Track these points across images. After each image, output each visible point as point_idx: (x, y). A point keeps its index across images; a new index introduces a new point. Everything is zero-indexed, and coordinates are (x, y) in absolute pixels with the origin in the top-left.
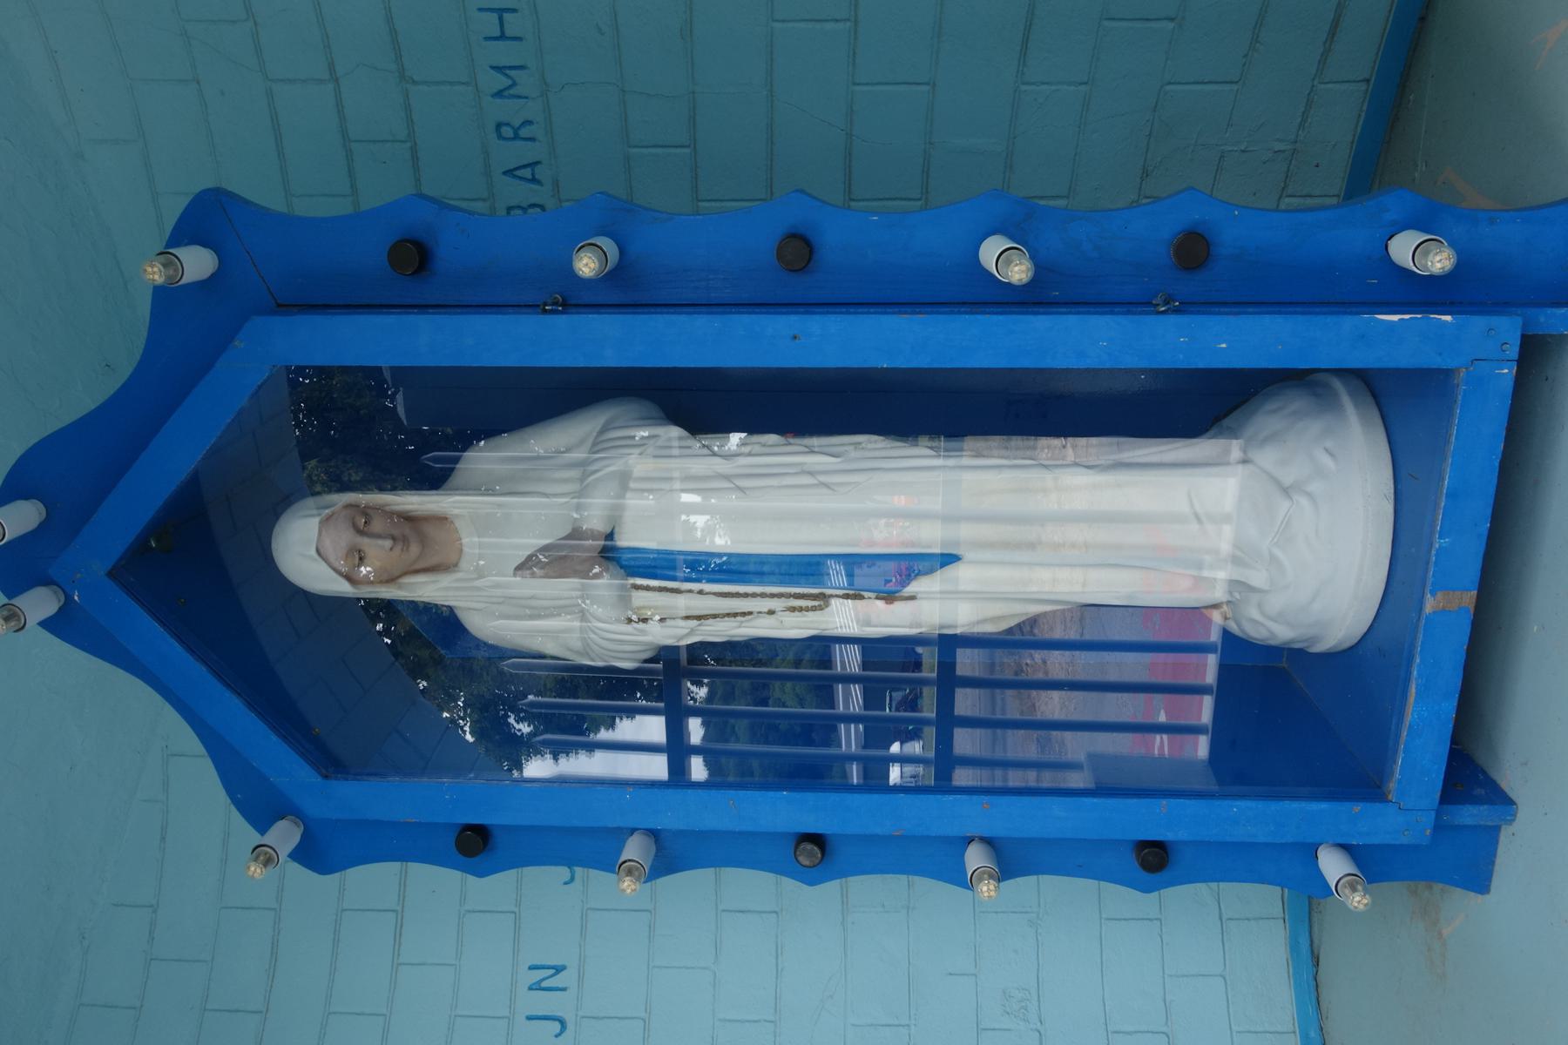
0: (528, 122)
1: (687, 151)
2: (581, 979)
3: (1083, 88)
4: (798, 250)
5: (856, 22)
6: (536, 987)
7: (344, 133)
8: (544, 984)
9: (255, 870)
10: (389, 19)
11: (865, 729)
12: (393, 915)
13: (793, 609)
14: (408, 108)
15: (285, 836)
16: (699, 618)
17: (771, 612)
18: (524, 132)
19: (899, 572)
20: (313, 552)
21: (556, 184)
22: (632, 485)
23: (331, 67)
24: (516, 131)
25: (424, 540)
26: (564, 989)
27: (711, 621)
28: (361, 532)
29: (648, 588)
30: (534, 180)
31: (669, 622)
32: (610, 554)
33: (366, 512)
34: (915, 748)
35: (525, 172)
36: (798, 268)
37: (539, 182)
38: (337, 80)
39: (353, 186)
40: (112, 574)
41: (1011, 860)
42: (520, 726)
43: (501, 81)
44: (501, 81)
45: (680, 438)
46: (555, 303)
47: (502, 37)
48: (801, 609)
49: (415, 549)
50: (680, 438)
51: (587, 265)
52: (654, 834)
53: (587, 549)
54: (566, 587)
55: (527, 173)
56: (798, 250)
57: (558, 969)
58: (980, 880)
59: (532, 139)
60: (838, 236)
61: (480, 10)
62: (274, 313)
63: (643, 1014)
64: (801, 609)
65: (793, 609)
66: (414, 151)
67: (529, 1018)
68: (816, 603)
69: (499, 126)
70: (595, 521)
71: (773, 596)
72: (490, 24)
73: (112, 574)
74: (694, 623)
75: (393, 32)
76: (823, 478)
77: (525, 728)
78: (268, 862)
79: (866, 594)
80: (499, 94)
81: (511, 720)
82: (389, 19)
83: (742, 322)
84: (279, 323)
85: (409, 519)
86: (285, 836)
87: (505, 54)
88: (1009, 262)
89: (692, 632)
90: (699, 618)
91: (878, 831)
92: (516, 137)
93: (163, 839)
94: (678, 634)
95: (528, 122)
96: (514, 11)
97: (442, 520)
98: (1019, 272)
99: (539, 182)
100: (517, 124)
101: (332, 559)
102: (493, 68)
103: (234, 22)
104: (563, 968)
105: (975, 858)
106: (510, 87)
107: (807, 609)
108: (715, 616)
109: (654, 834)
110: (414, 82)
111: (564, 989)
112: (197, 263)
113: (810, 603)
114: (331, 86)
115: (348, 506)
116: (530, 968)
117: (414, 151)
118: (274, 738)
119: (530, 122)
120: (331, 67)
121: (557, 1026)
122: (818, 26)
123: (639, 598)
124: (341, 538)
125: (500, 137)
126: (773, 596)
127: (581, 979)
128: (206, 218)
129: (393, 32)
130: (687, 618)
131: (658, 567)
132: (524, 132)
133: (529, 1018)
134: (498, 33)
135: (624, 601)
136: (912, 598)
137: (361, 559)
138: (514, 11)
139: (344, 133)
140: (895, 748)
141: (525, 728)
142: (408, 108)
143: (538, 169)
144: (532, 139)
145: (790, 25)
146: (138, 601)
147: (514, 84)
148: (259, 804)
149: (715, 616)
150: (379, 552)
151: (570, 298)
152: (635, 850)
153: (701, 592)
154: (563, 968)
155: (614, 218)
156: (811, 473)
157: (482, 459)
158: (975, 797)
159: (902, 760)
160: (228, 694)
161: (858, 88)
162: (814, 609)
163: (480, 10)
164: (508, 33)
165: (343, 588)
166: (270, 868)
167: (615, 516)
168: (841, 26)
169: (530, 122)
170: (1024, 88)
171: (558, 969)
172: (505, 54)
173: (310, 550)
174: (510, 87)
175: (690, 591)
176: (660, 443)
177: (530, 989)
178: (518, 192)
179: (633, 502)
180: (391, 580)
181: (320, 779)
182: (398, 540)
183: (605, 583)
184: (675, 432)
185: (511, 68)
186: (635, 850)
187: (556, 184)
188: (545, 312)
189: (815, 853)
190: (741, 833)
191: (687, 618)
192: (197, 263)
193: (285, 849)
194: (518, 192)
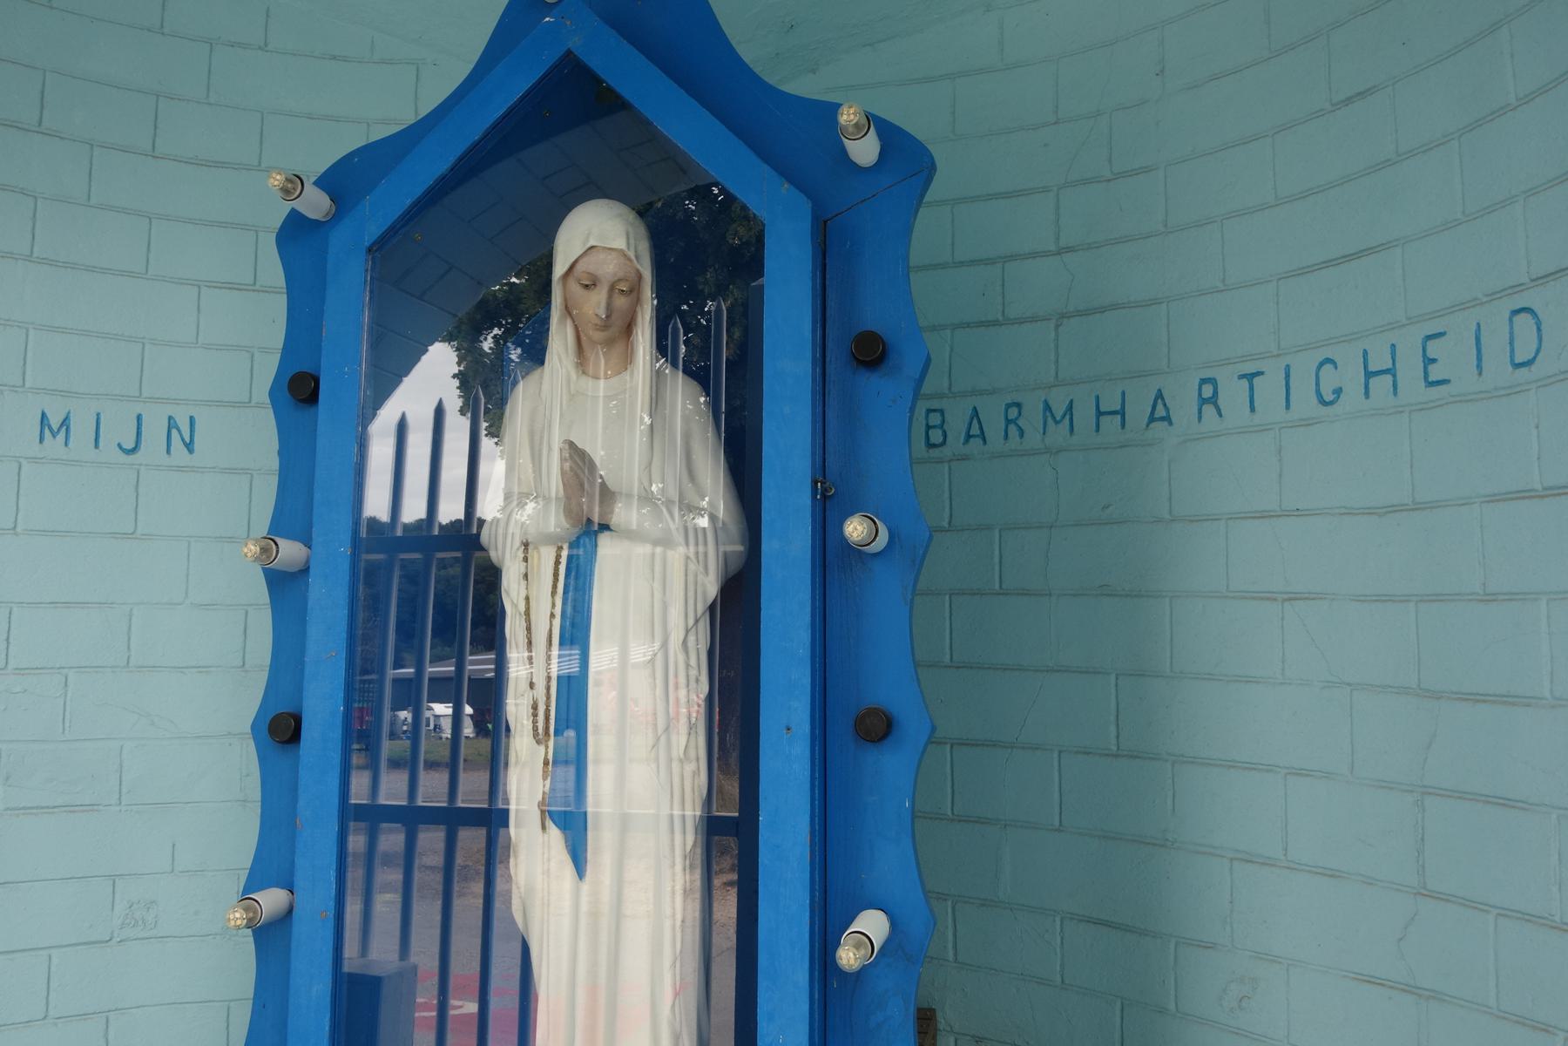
0: (1022, 433)
1: (997, 586)
2: (180, 469)
3: (1059, 979)
4: (877, 727)
5: (1116, 756)
6: (172, 424)
7: (1013, 257)
8: (174, 432)
9: (277, 180)
10: (1115, 307)
11: (489, 679)
12: (250, 280)
13: (535, 707)
14: (1034, 319)
15: (316, 204)
16: (527, 613)
17: (532, 685)
18: (1012, 429)
19: (571, 821)
20: (592, 243)
21: (965, 458)
22: (659, 550)
23: (1070, 249)
24: (1014, 421)
25: (609, 343)
26: (168, 451)
27: (524, 624)
28: (612, 288)
29: (557, 563)
30: (969, 437)
31: (523, 583)
32: (588, 531)
33: (634, 291)
34: (468, 730)
35: (976, 430)
36: (855, 727)
37: (967, 441)
38: (1059, 253)
39: (962, 264)
40: (569, 53)
41: (271, 936)
42: (490, 339)
43: (1059, 411)
44: (1059, 411)
45: (704, 593)
46: (825, 490)
47: (1099, 414)
48: (535, 715)
49: (598, 336)
50: (704, 593)
51: (855, 529)
52: (305, 571)
53: (591, 509)
54: (554, 485)
55: (975, 430)
56: (877, 727)
57: (189, 446)
58: (246, 910)
59: (1006, 436)
60: (890, 768)
61: (1123, 394)
62: (815, 218)
63: (139, 531)
64: (535, 715)
65: (535, 707)
66: (995, 323)
67: (139, 418)
68: (540, 731)
69: (1018, 405)
70: (625, 514)
71: (548, 688)
72: (1111, 402)
73: (569, 53)
74: (522, 608)
75: (1102, 310)
76: (663, 739)
77: (487, 345)
78: (286, 191)
79: (548, 782)
80: (1047, 407)
81: (496, 331)
82: (1115, 307)
83: (802, 677)
84: (805, 225)
85: (629, 329)
86: (316, 204)
87: (1085, 414)
88: (858, 946)
89: (515, 606)
90: (527, 613)
91: (301, 803)
92: (1008, 422)
93: (334, 58)
94: (512, 591)
95: (1022, 433)
96: (1123, 426)
97: (627, 360)
98: (848, 957)
99: (967, 441)
100: (1020, 422)
101: (585, 259)
102: (1071, 402)
103: (1110, 161)
104: (191, 451)
105: (271, 900)
106: (1054, 417)
107: (535, 722)
108: (529, 629)
109: (305, 571)
110: (1057, 327)
111: (168, 451)
112: (865, 150)
113: (541, 725)
114: (1053, 248)
115: (640, 277)
116: (191, 418)
117: (995, 323)
118: (409, 202)
119: (1022, 435)
120: (1070, 249)
121: (130, 445)
122: (1113, 718)
123: (546, 556)
124: (608, 268)
125: (1008, 406)
126: (548, 688)
127: (180, 469)
128: (906, 157)
129: (1102, 310)
130: (527, 599)
131: (577, 580)
132: (1012, 428)
133: (139, 418)
134: (1102, 409)
135: (548, 539)
136: (544, 827)
137: (586, 286)
138: (1123, 426)
139: (1013, 257)
140: (468, 710)
141: (487, 345)
142: (1034, 319)
143: (979, 441)
144: (1006, 436)
145: (1113, 691)
146: (542, 78)
147: (1057, 422)
148: (344, 181)
149: (529, 629)
150: (594, 304)
151: (829, 504)
152: (290, 551)
153: (552, 616)
154: (191, 451)
155: (906, 549)
156: (667, 729)
157: (685, 399)
158: (332, 904)
159: (457, 717)
160: (452, 160)
161: (1056, 755)
162: (535, 729)
163: (1123, 394)
164: (1103, 419)
165: (559, 270)
166: (280, 194)
167: (631, 535)
168: (1114, 741)
169: (1022, 435)
170: (1058, 920)
171: (189, 446)
172: (1085, 414)
173: (597, 238)
174: (1054, 417)
175: (554, 605)
176: (700, 577)
177: (170, 418)
178: (957, 423)
179: (642, 550)
180: (567, 310)
181: (367, 244)
182: (605, 325)
183: (556, 522)
184: (712, 589)
185: (1071, 420)
186: (290, 551)
187: (965, 458)
188: (815, 483)
189: (283, 729)
190: (302, 663)
191: (527, 599)
192: (865, 150)
193: (301, 206)
194: (957, 423)
